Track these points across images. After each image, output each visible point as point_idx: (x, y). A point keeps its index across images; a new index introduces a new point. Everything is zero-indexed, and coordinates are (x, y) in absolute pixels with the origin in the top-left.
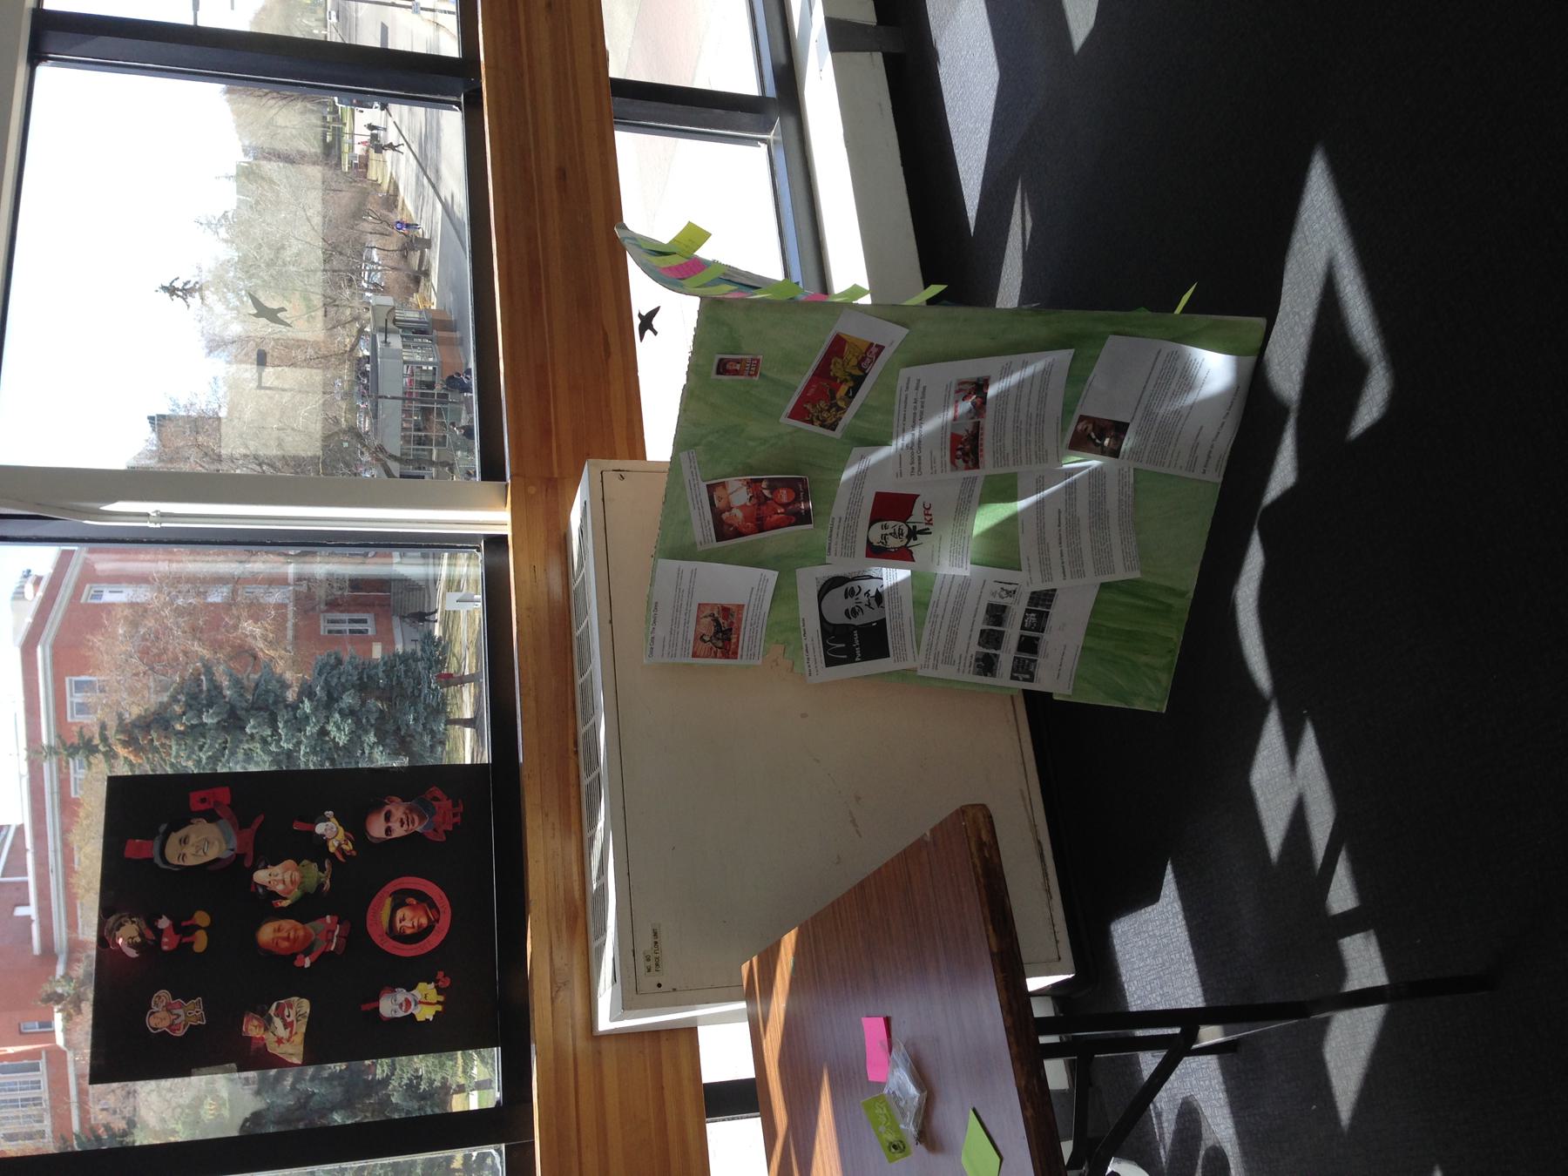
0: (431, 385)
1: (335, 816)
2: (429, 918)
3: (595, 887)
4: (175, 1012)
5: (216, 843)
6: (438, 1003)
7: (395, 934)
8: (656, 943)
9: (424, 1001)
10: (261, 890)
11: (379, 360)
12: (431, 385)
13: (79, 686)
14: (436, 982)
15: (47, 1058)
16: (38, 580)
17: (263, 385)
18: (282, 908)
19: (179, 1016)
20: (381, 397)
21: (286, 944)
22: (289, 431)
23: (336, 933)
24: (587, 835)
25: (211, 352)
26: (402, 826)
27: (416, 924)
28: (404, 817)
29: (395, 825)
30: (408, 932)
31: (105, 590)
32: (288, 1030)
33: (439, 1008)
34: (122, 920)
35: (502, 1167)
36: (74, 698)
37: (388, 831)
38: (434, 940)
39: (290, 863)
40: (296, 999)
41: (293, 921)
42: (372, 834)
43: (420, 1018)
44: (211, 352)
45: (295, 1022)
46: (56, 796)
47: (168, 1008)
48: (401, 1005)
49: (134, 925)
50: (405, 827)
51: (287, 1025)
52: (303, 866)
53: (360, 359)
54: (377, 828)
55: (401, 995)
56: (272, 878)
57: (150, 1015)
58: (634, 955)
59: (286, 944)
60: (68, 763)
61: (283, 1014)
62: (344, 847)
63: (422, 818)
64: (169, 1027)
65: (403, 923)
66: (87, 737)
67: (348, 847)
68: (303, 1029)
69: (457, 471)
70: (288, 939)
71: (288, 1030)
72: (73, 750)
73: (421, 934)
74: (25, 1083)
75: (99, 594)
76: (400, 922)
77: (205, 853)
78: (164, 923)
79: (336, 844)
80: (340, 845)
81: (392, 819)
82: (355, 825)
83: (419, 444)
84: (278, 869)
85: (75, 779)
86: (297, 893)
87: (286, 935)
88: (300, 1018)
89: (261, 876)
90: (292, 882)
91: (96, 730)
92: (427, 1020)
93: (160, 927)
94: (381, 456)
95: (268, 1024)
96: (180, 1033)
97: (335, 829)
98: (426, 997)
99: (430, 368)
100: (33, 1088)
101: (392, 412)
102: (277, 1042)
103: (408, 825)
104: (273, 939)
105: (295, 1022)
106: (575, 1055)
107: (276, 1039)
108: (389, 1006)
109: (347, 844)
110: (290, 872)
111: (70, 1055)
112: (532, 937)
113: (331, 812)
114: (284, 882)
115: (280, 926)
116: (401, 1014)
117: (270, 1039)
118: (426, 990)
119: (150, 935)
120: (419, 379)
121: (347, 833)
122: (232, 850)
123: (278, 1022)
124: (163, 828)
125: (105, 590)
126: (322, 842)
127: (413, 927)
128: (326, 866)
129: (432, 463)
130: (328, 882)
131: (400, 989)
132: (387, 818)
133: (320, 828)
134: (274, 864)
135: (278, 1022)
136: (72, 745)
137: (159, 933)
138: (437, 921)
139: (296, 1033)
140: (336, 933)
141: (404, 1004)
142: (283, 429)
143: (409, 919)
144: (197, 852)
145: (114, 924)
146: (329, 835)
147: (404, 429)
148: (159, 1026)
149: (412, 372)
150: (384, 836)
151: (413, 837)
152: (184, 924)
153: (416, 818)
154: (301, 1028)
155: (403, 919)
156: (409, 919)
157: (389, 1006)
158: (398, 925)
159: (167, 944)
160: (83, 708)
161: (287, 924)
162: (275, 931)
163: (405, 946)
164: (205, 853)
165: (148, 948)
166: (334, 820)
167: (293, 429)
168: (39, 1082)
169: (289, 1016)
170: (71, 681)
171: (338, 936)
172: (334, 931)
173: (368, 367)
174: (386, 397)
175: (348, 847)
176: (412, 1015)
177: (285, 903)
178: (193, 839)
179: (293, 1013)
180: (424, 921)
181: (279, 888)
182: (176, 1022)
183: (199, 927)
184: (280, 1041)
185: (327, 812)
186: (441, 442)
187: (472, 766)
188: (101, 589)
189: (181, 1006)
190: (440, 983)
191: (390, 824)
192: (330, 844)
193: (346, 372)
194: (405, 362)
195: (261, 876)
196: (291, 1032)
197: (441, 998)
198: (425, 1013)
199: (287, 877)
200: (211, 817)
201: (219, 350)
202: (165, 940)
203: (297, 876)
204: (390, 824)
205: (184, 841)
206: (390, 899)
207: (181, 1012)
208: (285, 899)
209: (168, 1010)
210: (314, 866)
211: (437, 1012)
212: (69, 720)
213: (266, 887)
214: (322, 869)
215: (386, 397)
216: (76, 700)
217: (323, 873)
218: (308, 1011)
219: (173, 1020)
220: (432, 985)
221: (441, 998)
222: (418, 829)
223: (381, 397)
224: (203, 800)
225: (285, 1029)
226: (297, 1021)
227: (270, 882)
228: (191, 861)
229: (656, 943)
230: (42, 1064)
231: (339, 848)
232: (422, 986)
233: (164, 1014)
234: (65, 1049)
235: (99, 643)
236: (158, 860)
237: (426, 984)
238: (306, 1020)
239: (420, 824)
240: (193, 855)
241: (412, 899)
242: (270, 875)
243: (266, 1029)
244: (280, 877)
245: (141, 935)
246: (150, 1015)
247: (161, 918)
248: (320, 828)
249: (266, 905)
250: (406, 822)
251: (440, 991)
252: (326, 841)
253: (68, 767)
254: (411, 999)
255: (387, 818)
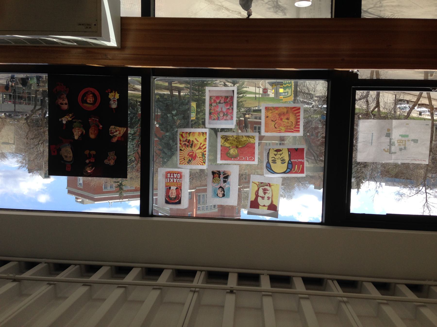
0: (10, 95)
1: (61, 118)
2: (90, 94)
3: (76, 44)
4: (110, 158)
5: (67, 148)
6: (115, 92)
7: (93, 104)
8: (83, 25)
9: (114, 96)
10: (80, 138)
11: (3, 110)
12: (10, 95)
13: (106, 188)
14: (109, 93)
15: (198, 193)
16: (76, 198)
17: (13, 143)
18: (85, 133)
19: (112, 158)
20: (15, 110)
21: (96, 132)
22: (28, 136)
23: (94, 119)
24: (61, 45)
25: (5, 157)
26: (65, 100)
27: (92, 97)
28: (62, 100)
29: (64, 102)
30: (93, 99)
31: (79, 183)
32: (118, 131)
33: (116, 92)
34: (85, 171)
35: (159, 78)
36: (109, 189)
37: (66, 104)
38: (97, 93)
39: (73, 130)
40: (110, 129)
41: (90, 130)
42: (67, 108)
43: (118, 97)
44: (5, 157)
45: (116, 129)
46: (134, 192)
47: (109, 160)
48: (114, 102)
49: (87, 168)
50: (65, 99)
51: (116, 132)
52: (74, 127)
53: (5, 116)
54: (65, 107)
55: (112, 102)
56: (77, 135)
57: (110, 164)
58: (86, 32)
59: (96, 132)
60: (124, 190)
61: (113, 132)
62: (70, 116)
63: (62, 95)
64: (114, 160)
65: (91, 101)
66: (118, 186)
67: (71, 115)
68: (118, 127)
69: (38, 89)
70: (94, 131)
71: (118, 131)
72: (121, 189)
73: (94, 96)
74: (203, 198)
75: (80, 184)
76: (91, 101)
77: (69, 152)
78: (87, 161)
79: (69, 118)
80: (70, 117)
81: (62, 103)
82: (64, 113)
83: (30, 100)
84: (75, 133)
85: (130, 188)
86: (82, 129)
87: (93, 131)
88: (115, 128)
89: (76, 137)
90: (79, 129)
91: (117, 184)
92: (119, 96)
93: (88, 162)
94: (34, 111)
95: (115, 136)
96: (116, 157)
97: (65, 118)
98: (113, 96)
99: (4, 95)
100: (204, 196)
101: (19, 108)
102: (120, 134)
103: (64, 98)
104: (94, 135)
105: (116, 129)
106: (134, 55)
107: (119, 134)
108: (114, 106)
109: (70, 115)
110: (76, 130)
111: (197, 188)
112: (92, 64)
113: (60, 119)
114: (79, 132)
115: (91, 133)
116: (116, 103)
117: (118, 136)
118: (111, 96)
119: (90, 165)
120: (9, 99)
121: (67, 115)
122: (69, 145)
123: (115, 134)
124: (63, 162)
125: (79, 183)
126: (68, 122)
127: (92, 98)
128: (74, 121)
129: (36, 97)
130: (79, 120)
131: (110, 102)
132: (62, 104)
133: (64, 122)
134: (74, 134)
135: (115, 134)
136: (120, 189)
137: (90, 162)
138: (91, 92)
139: (119, 129)
140: (94, 119)
141: (114, 102)
142: (27, 138)
143: (90, 99)
144: (69, 153)
145: (86, 173)
146: (66, 120)
147: (26, 104)
148: (113, 162)
149: (7, 101)
150: (67, 105)
151: (68, 97)
152: (88, 156)
153: (62, 96)
154: (118, 128)
155: (90, 101)
156: (90, 99)
157: (114, 106)
158: (92, 102)
159: (93, 160)
160: (111, 187)
161: (91, 131)
162: (92, 134)
163: (98, 100)
164: (69, 152)
165: (92, 165)
166: (62, 119)
167: (27, 135)
168: (203, 195)
169: (114, 131)
170: (104, 190)
171: (95, 118)
172: (93, 119)
173: (7, 114)
174: (15, 109)
175: (71, 115)
176: (117, 100)
177: (84, 132)
178: (66, 154)
179: (113, 130)
180: (91, 95)
181: (80, 133)
182: (113, 158)
183: (89, 153)
184: (120, 133)
185: (60, 120)
186: (30, 94)
187: (142, 92)
188: (79, 184)
189: (110, 157)
190: (109, 92)
191: (64, 103)
192: (69, 120)
193: (8, 120)
194: (3, 103)
195: (76, 137)
196: (118, 130)
197: (114, 92)
198: (117, 96)
199: (77, 131)
200: (59, 150)
201: (4, 154)
202: (92, 161)
203: (77, 129)
204: (64, 103)
205: (66, 157)
206: (84, 104)
207: (111, 157)
208: (83, 131)
209: (110, 160)
210: (75, 124)
211: (117, 93)
212: (114, 190)
213: (79, 136)
214: (75, 122)
215: (15, 109)
216: (109, 189)
217: (76, 122)
218: (114, 126)
219: (112, 159)
220: (110, 94)
221: (114, 92)
222: (66, 96)
223: (15, 110)
224: (54, 152)
225: (117, 132)
226: (116, 129)
227: (78, 135)
228: (71, 155)
229: (83, 25)
230: (199, 194)
231: (71, 117)
232: (110, 97)
233: (110, 161)
234: (196, 189)
235: (93, 183)
236: (71, 163)
237: (109, 96)
238: (116, 127)
239: (64, 95)
240: (70, 154)
241: (85, 98)
242: (76, 135)
243: (116, 137)
244: (77, 133)
245: (90, 167)
246: (110, 164)
247: (86, 162)
248: (64, 122)
249: (84, 136)
250: (63, 99)
251: (112, 92)
252: (68, 121)
253: (125, 190)
254: (113, 100)
255: (62, 104)
